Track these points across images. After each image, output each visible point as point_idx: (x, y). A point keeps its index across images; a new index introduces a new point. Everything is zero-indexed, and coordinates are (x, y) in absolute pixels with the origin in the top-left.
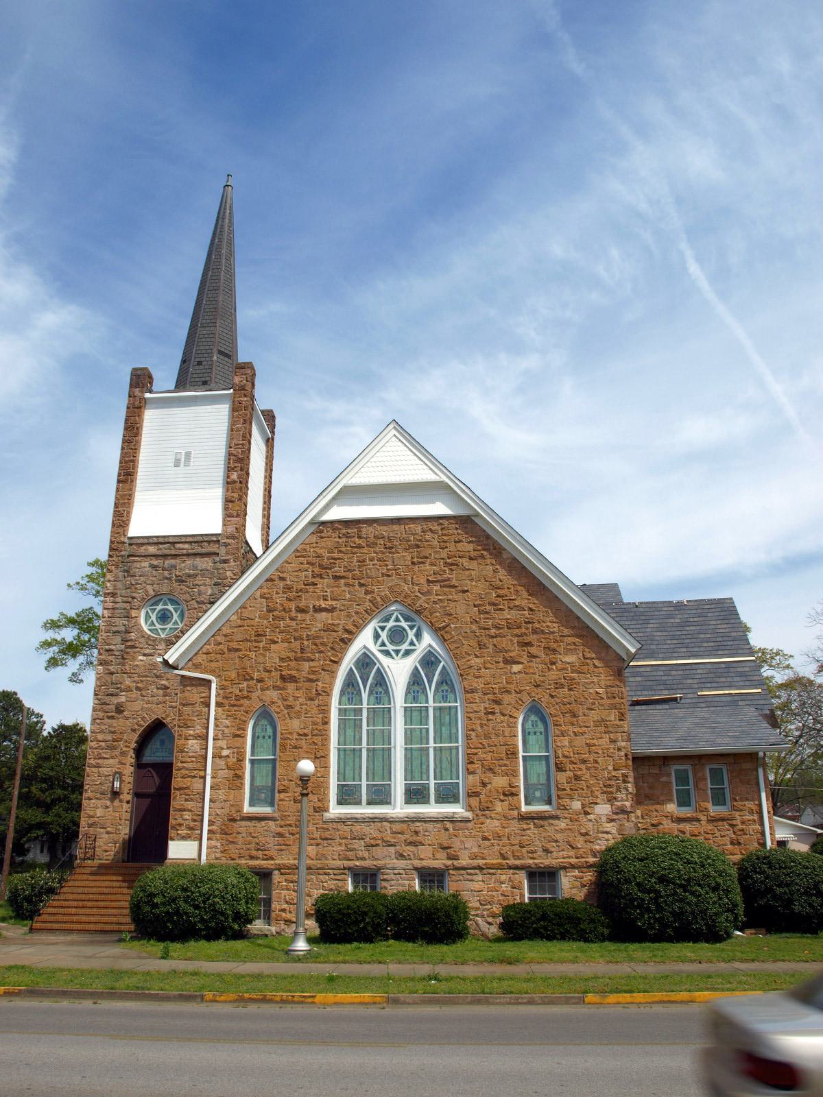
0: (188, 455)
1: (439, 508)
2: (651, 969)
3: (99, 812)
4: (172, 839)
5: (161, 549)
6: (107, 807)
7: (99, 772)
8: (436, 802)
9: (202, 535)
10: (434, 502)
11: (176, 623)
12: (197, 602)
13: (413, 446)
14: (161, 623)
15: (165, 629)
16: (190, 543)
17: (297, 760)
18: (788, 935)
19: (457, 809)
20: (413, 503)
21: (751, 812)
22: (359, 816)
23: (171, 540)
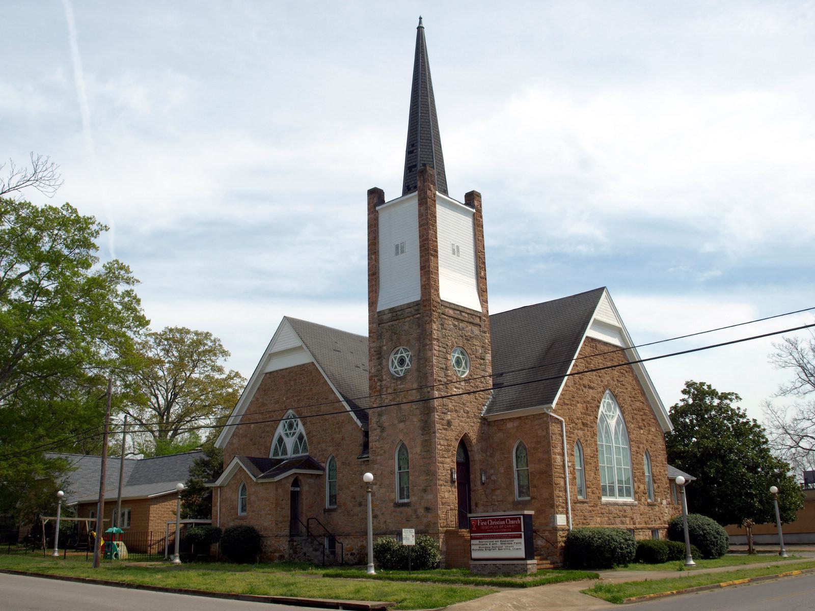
0: (397, 254)
1: (616, 341)
2: (732, 569)
3: (447, 495)
4: (557, 514)
5: (455, 314)
6: (450, 491)
7: (443, 467)
8: (619, 496)
9: (473, 310)
10: (615, 338)
11: (396, 367)
12: (476, 356)
13: (611, 302)
14: (401, 366)
15: (402, 370)
16: (468, 314)
17: (362, 474)
18: (269, 570)
19: (629, 500)
20: (602, 333)
21: (563, 508)
22: (611, 502)
23: (461, 309)
